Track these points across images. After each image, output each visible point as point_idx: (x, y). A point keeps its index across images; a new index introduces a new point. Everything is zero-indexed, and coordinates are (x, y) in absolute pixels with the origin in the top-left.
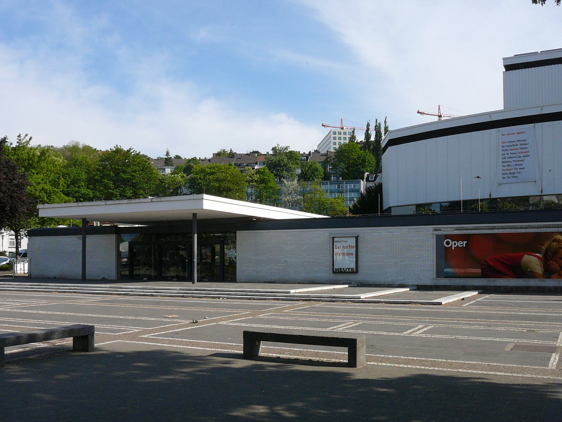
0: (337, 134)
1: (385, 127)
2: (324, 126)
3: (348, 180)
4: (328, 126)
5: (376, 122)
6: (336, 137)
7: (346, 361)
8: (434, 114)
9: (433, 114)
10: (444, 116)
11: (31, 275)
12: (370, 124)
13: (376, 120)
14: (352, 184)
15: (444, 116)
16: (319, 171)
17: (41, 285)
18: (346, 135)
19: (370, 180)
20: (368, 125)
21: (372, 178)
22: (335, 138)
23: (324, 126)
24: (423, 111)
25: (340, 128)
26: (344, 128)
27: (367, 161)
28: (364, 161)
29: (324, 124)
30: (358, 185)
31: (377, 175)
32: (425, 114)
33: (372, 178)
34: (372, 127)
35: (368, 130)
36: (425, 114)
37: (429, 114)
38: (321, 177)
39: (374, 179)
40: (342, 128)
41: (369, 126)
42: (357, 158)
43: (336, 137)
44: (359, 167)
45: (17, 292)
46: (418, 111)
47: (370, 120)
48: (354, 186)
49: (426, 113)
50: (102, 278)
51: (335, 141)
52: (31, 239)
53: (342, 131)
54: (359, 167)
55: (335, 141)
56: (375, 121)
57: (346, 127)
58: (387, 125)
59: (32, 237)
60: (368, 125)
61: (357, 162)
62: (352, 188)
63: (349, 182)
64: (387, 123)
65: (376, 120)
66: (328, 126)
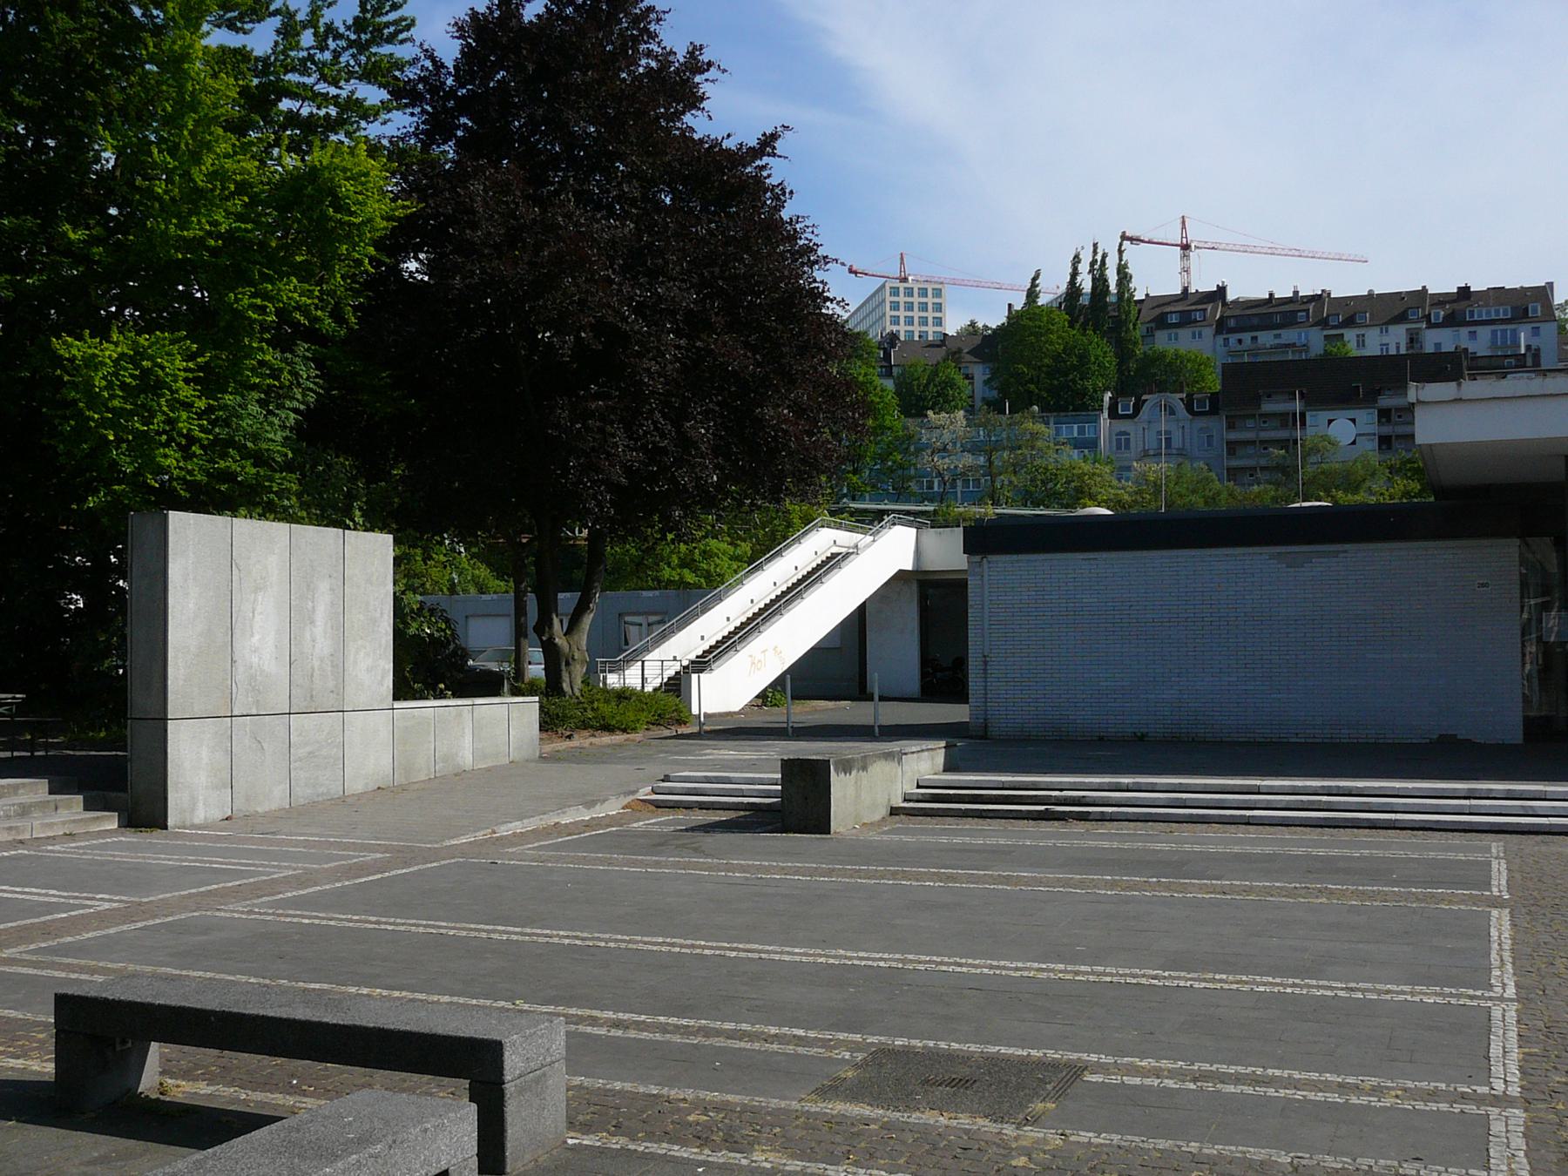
0: (902, 294)
1: (1119, 264)
2: (856, 273)
3: (1062, 414)
4: (866, 274)
5: (1095, 252)
6: (912, 303)
7: (42, 1067)
8: (1169, 242)
9: (1165, 241)
10: (1196, 247)
11: (986, 727)
12: (1081, 257)
13: (1095, 246)
14: (1076, 426)
15: (1196, 247)
16: (959, 388)
17: (1491, 790)
18: (927, 296)
19: (1120, 412)
20: (1077, 260)
21: (1126, 408)
22: (895, 306)
23: (856, 273)
24: (1138, 234)
25: (1177, 245)
26: (910, 278)
27: (1093, 359)
28: (1084, 358)
29: (854, 268)
30: (1092, 430)
31: (1144, 397)
32: (1143, 241)
33: (1126, 408)
34: (1084, 267)
35: (1075, 274)
36: (1143, 241)
37: (1155, 240)
38: (965, 404)
39: (1131, 412)
40: (905, 280)
41: (1079, 262)
42: (1064, 351)
43: (912, 303)
44: (1071, 377)
45: (1313, 834)
46: (1124, 233)
47: (1083, 248)
48: (1082, 431)
49: (1146, 239)
50: (1435, 737)
51: (896, 313)
52: (986, 565)
53: (902, 286)
54: (1071, 377)
55: (896, 313)
56: (1092, 248)
57: (915, 275)
58: (1124, 259)
59: (991, 558)
60: (1077, 260)
61: (1065, 362)
62: (1076, 435)
63: (1065, 419)
64: (1124, 255)
65: (1095, 246)
66: (866, 274)
